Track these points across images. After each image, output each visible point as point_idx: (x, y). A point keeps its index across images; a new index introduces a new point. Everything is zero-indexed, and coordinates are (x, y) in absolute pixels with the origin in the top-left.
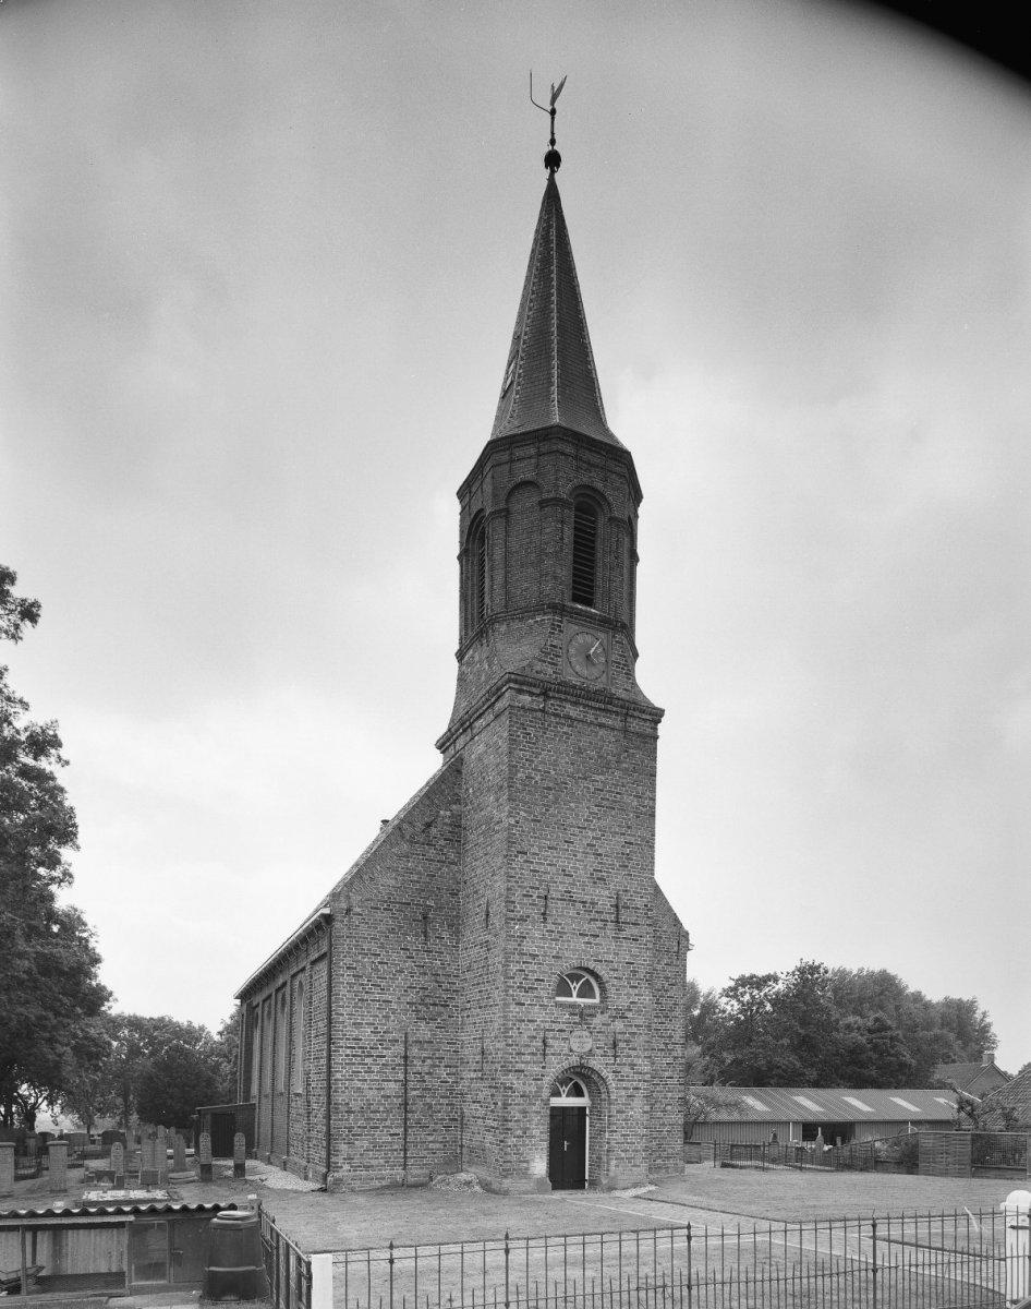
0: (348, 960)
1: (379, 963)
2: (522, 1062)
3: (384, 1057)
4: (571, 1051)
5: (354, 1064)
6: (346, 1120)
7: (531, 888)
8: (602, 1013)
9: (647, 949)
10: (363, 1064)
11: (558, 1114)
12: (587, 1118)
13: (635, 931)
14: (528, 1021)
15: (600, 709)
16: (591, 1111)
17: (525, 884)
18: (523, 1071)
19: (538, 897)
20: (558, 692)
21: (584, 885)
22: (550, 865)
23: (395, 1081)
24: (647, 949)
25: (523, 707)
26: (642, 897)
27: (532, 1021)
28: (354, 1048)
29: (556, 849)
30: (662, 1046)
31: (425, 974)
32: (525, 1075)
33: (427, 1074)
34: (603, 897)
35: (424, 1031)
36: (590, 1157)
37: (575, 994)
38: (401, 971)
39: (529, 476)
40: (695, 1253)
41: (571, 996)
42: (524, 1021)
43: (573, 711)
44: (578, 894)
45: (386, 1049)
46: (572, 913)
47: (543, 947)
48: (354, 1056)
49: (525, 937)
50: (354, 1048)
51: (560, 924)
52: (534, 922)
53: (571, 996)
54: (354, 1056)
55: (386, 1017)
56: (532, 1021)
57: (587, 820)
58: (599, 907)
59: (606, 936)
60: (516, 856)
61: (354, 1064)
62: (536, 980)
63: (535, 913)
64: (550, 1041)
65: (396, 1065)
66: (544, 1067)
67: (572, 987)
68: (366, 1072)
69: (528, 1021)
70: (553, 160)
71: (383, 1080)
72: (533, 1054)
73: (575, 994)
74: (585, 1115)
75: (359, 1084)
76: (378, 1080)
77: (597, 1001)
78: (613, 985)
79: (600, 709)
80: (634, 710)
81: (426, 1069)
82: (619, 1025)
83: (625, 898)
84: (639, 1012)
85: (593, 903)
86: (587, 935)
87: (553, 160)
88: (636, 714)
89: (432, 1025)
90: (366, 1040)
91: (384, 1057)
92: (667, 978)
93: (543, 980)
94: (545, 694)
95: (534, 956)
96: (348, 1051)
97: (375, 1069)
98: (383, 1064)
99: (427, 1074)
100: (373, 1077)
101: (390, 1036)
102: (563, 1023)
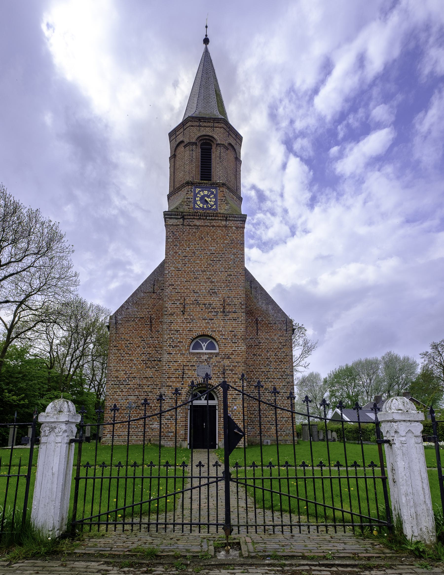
0: (115, 343)
1: (129, 344)
2: (171, 382)
3: (129, 384)
4: (198, 375)
5: (115, 388)
6: (110, 413)
7: (176, 300)
8: (216, 356)
9: (242, 324)
10: (119, 388)
11: (195, 410)
12: (217, 411)
13: (235, 315)
14: (174, 362)
15: (212, 219)
16: (218, 407)
17: (173, 299)
18: (171, 386)
19: (180, 304)
20: (189, 216)
21: (204, 297)
22: (186, 289)
23: (134, 396)
24: (242, 324)
25: (172, 225)
26: (238, 299)
27: (176, 362)
28: (115, 381)
29: (189, 282)
30: (279, 376)
31: (150, 347)
32: (172, 388)
33: (150, 392)
34: (216, 301)
35: (149, 373)
36: (219, 432)
37: (204, 348)
38: (139, 347)
39: (181, 139)
40: (177, 498)
41: (202, 349)
42: (172, 362)
43: (198, 223)
44: (201, 300)
45: (130, 381)
46: (198, 309)
47: (183, 326)
48: (115, 384)
49: (173, 323)
50: (115, 381)
51: (192, 315)
52: (177, 315)
53: (202, 349)
54: (115, 384)
55: (131, 367)
56: (176, 362)
57: (206, 268)
58: (214, 306)
59: (218, 319)
60: (168, 287)
61: (115, 388)
62: (178, 342)
63: (178, 311)
64: (187, 371)
65: (135, 388)
66: (182, 384)
67: (203, 345)
68: (120, 392)
69: (174, 362)
70: (206, 41)
71: (128, 395)
72: (176, 378)
73: (204, 348)
74: (216, 409)
75: (117, 397)
76: (126, 395)
77: (217, 351)
78: (222, 342)
79: (212, 219)
80: (230, 217)
81: (149, 390)
82: (227, 362)
83: (228, 301)
84: (238, 355)
85: (210, 304)
86: (207, 319)
87: (206, 41)
88: (231, 219)
89: (153, 370)
90: (121, 377)
91: (129, 384)
92: (280, 343)
93: (182, 342)
94: (183, 218)
95: (177, 331)
96: (112, 382)
97: (125, 390)
98: (129, 388)
99: (150, 392)
100: (124, 394)
101: (133, 375)
102: (194, 362)
